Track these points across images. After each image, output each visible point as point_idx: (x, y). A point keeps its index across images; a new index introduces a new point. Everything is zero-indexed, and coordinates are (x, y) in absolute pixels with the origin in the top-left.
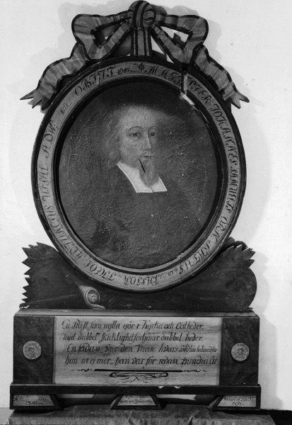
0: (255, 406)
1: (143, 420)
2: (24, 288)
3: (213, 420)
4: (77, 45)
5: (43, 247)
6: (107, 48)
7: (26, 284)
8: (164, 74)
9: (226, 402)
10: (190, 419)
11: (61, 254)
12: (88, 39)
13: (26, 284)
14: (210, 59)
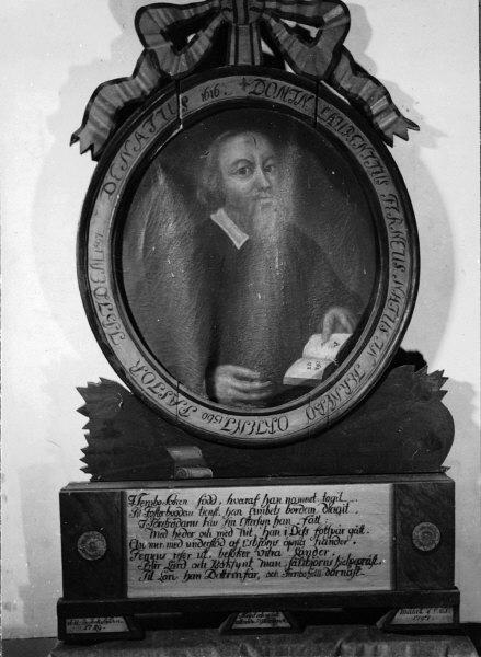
0: (451, 622)
1: (264, 648)
2: (406, 139)
3: (375, 644)
4: (144, 54)
5: (105, 384)
6: (189, 58)
7: (86, 444)
8: (284, 93)
9: (404, 617)
10: (339, 642)
11: (138, 396)
12: (163, 47)
13: (86, 444)
14: (357, 69)
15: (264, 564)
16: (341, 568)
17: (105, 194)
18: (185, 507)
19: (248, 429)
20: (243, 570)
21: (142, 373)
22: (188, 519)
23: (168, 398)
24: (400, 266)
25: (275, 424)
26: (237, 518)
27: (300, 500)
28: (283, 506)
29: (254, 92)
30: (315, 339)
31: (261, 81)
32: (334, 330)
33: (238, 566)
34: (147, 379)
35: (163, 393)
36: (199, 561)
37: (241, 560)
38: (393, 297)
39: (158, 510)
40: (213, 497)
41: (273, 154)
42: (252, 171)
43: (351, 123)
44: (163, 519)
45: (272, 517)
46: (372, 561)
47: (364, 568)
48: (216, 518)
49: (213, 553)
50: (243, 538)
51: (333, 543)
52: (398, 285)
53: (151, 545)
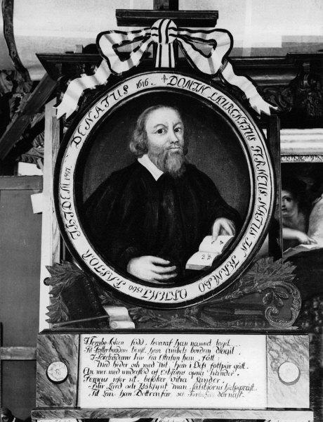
15: (175, 387)
16: (228, 392)
17: (74, 144)
18: (123, 347)
19: (160, 297)
20: (160, 391)
21: (90, 258)
22: (122, 354)
23: (107, 276)
24: (264, 192)
25: (178, 294)
26: (158, 355)
27: (201, 344)
28: (189, 348)
29: (170, 84)
30: (207, 239)
31: (175, 77)
32: (220, 233)
33: (157, 388)
34: (93, 262)
35: (104, 272)
36: (130, 384)
37: (159, 384)
38: (259, 212)
39: (104, 348)
40: (142, 341)
41: (181, 121)
42: (166, 132)
43: (231, 102)
44: (107, 354)
45: (181, 355)
46: (250, 389)
47: (245, 392)
48: (143, 355)
49: (141, 378)
50: (161, 369)
51: (223, 374)
52: (262, 204)
53: (98, 372)
